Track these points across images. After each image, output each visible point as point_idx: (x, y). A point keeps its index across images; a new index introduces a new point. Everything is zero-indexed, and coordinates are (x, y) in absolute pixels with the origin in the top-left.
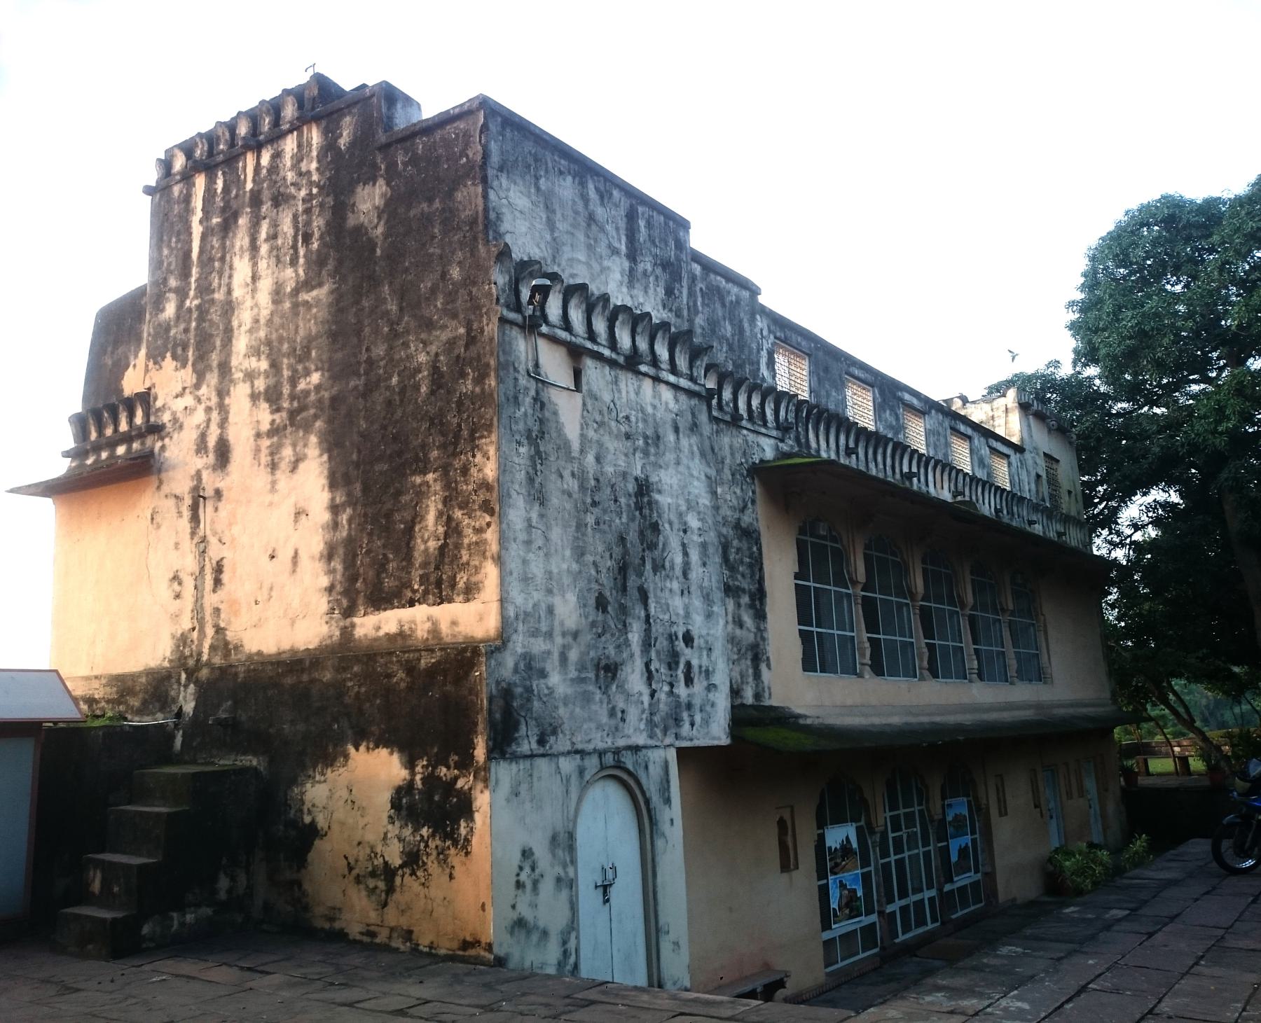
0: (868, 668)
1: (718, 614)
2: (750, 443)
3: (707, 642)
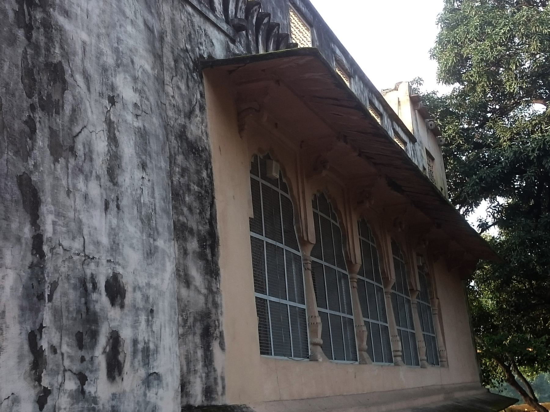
0: (319, 349)
1: (164, 251)
2: (197, 28)
3: (146, 298)
